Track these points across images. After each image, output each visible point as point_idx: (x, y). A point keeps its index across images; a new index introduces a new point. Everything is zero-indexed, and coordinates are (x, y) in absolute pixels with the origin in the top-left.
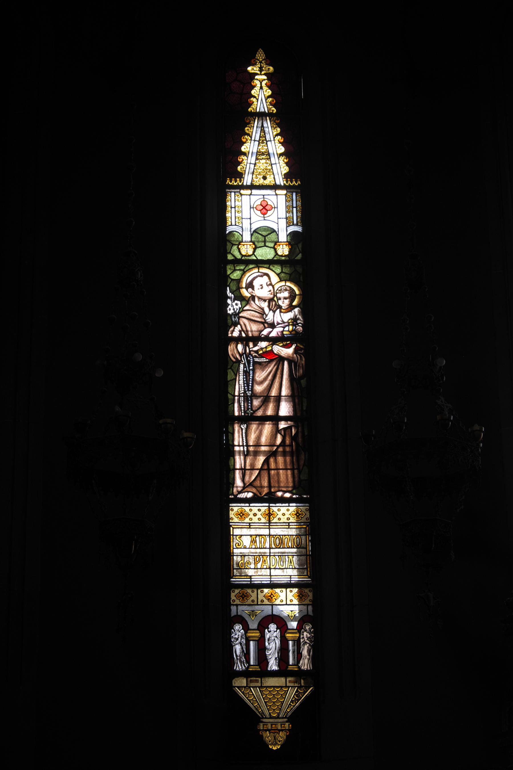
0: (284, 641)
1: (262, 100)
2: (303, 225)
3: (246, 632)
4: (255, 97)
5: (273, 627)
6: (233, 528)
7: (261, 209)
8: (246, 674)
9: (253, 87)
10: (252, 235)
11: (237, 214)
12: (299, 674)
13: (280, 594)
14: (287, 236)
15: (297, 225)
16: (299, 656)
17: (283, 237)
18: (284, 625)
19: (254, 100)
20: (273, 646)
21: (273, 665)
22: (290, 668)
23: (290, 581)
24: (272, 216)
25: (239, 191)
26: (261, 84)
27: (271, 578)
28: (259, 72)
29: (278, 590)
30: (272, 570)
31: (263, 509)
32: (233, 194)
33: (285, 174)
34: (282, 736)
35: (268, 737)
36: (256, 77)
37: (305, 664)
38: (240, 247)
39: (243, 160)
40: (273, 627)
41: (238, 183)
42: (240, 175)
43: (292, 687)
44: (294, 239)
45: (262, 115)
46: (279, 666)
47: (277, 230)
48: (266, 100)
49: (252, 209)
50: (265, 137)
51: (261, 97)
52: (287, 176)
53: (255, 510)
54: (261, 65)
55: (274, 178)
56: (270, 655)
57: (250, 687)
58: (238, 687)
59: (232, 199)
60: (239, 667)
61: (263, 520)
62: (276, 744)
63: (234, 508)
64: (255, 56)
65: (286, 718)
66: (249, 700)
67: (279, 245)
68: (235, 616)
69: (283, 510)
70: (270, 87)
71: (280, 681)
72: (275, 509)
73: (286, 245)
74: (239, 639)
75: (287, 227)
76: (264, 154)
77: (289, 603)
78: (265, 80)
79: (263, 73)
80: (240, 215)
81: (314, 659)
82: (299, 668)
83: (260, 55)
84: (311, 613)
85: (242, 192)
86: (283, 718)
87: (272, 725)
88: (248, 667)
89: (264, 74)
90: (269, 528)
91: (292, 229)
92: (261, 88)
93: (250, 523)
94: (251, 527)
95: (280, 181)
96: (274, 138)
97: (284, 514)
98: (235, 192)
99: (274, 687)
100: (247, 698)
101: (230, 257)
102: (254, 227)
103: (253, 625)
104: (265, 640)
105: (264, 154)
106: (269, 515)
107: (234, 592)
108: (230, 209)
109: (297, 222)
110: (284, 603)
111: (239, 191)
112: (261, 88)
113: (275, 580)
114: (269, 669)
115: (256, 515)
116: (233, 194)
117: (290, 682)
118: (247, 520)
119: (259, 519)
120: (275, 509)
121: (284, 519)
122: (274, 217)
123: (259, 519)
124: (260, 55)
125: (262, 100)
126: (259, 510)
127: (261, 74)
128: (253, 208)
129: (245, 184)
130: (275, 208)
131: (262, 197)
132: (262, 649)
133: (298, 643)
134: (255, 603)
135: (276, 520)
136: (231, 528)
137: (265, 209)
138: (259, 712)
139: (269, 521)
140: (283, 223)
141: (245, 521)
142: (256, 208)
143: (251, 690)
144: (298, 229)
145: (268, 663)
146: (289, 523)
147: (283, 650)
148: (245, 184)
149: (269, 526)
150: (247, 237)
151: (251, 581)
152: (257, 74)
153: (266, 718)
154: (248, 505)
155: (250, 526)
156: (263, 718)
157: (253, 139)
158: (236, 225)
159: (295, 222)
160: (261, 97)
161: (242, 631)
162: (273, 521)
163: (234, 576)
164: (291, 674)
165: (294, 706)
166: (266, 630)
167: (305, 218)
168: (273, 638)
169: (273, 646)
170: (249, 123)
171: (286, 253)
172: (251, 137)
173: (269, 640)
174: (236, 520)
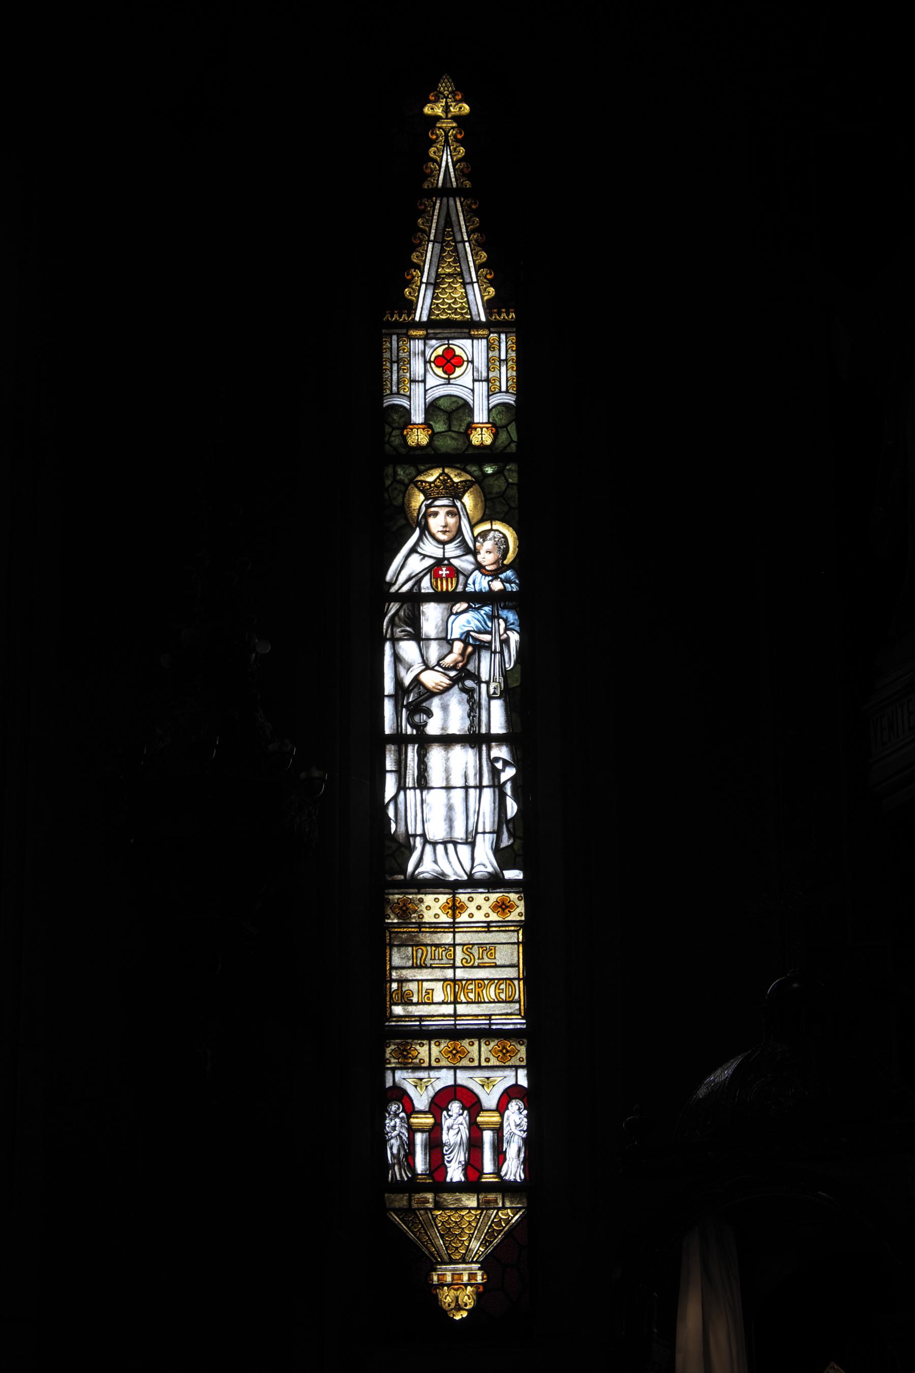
0: (475, 1130)
4: (434, 161)
5: (455, 1107)
6: (391, 933)
9: (432, 143)
12: (504, 1187)
13: (469, 1048)
15: (507, 392)
16: (500, 1156)
18: (476, 1103)
21: (455, 1173)
22: (486, 1179)
23: (490, 1024)
24: (464, 378)
28: (443, 115)
29: (465, 1043)
30: (457, 970)
32: (395, 337)
37: (513, 1169)
39: (413, 277)
40: (455, 1107)
42: (411, 307)
46: (465, 1175)
47: (471, 402)
49: (428, 365)
50: (454, 235)
54: (446, 102)
55: (425, 395)
64: (437, 86)
67: (475, 429)
69: (479, 898)
73: (487, 428)
75: (489, 396)
77: (484, 1064)
81: (528, 1164)
84: (523, 1081)
85: (413, 333)
90: (454, 933)
91: (496, 400)
92: (447, 141)
97: (479, 908)
102: (433, 395)
104: (442, 1129)
109: (507, 387)
110: (476, 1063)
112: (447, 141)
113: (462, 1023)
116: (395, 337)
122: (467, 380)
123: (436, 916)
131: (419, 832)
132: (435, 1146)
137: (449, 362)
139: (454, 897)
144: (510, 399)
145: (447, 1173)
147: (474, 1145)
149: (454, 927)
150: (418, 417)
159: (504, 388)
166: (445, 1113)
167: (525, 382)
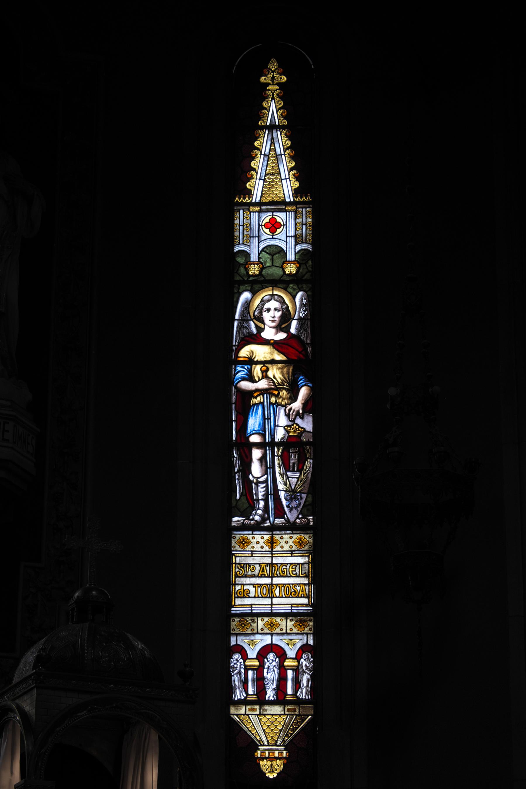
0: (282, 670)
1: (273, 111)
2: (313, 244)
3: (244, 662)
6: (236, 557)
7: (272, 215)
8: (245, 702)
10: (259, 254)
11: (245, 233)
12: (298, 702)
14: (296, 254)
17: (291, 257)
19: (253, 173)
20: (271, 675)
21: (270, 695)
25: (248, 208)
26: (273, 95)
27: (272, 607)
31: (266, 537)
33: (295, 189)
34: (279, 765)
35: (264, 765)
36: (269, 87)
37: (303, 694)
38: (247, 266)
40: (271, 656)
41: (247, 200)
42: (249, 193)
43: (290, 715)
44: (302, 257)
45: (272, 127)
47: (285, 249)
48: (277, 112)
51: (273, 111)
52: (296, 192)
53: (258, 538)
56: (290, 591)
57: (248, 715)
58: (237, 715)
59: (240, 217)
60: (239, 695)
61: (266, 548)
62: (272, 772)
63: (236, 536)
65: (283, 746)
66: (247, 728)
68: (234, 645)
70: (281, 98)
71: (277, 709)
72: (277, 537)
74: (238, 669)
76: (273, 170)
78: (277, 90)
79: (275, 82)
80: (248, 233)
81: (313, 690)
82: (297, 697)
83: (273, 65)
84: (311, 642)
85: (252, 208)
86: (280, 745)
87: (269, 753)
88: (246, 698)
89: (276, 84)
90: (272, 557)
93: (252, 551)
94: (254, 555)
95: (289, 196)
96: (284, 152)
98: (243, 209)
99: (272, 715)
100: (245, 726)
101: (238, 278)
103: (252, 653)
105: (273, 170)
106: (272, 543)
107: (234, 621)
108: (238, 227)
110: (284, 631)
111: (248, 208)
114: (267, 699)
115: (257, 543)
116: (241, 211)
117: (289, 710)
118: (249, 548)
119: (262, 547)
120: (277, 537)
121: (286, 547)
123: (262, 547)
124: (273, 65)
125: (273, 111)
126: (262, 538)
127: (273, 85)
128: (262, 225)
129: (253, 201)
130: (284, 225)
132: (260, 681)
133: (296, 670)
134: (255, 631)
135: (278, 548)
136: (234, 557)
137: (273, 226)
138: (257, 740)
140: (292, 241)
141: (247, 549)
142: (264, 226)
143: (249, 717)
144: (308, 247)
146: (292, 551)
147: (282, 679)
148: (253, 201)
151: (252, 610)
152: (268, 84)
153: (264, 745)
154: (250, 532)
155: (252, 554)
156: (261, 745)
157: (263, 153)
158: (243, 244)
160: (273, 111)
161: (241, 660)
162: (274, 550)
163: (235, 605)
164: (290, 703)
165: (292, 734)
168: (272, 667)
169: (271, 675)
170: (258, 137)
171: (294, 271)
172: (261, 152)
173: (269, 667)
174: (238, 548)
